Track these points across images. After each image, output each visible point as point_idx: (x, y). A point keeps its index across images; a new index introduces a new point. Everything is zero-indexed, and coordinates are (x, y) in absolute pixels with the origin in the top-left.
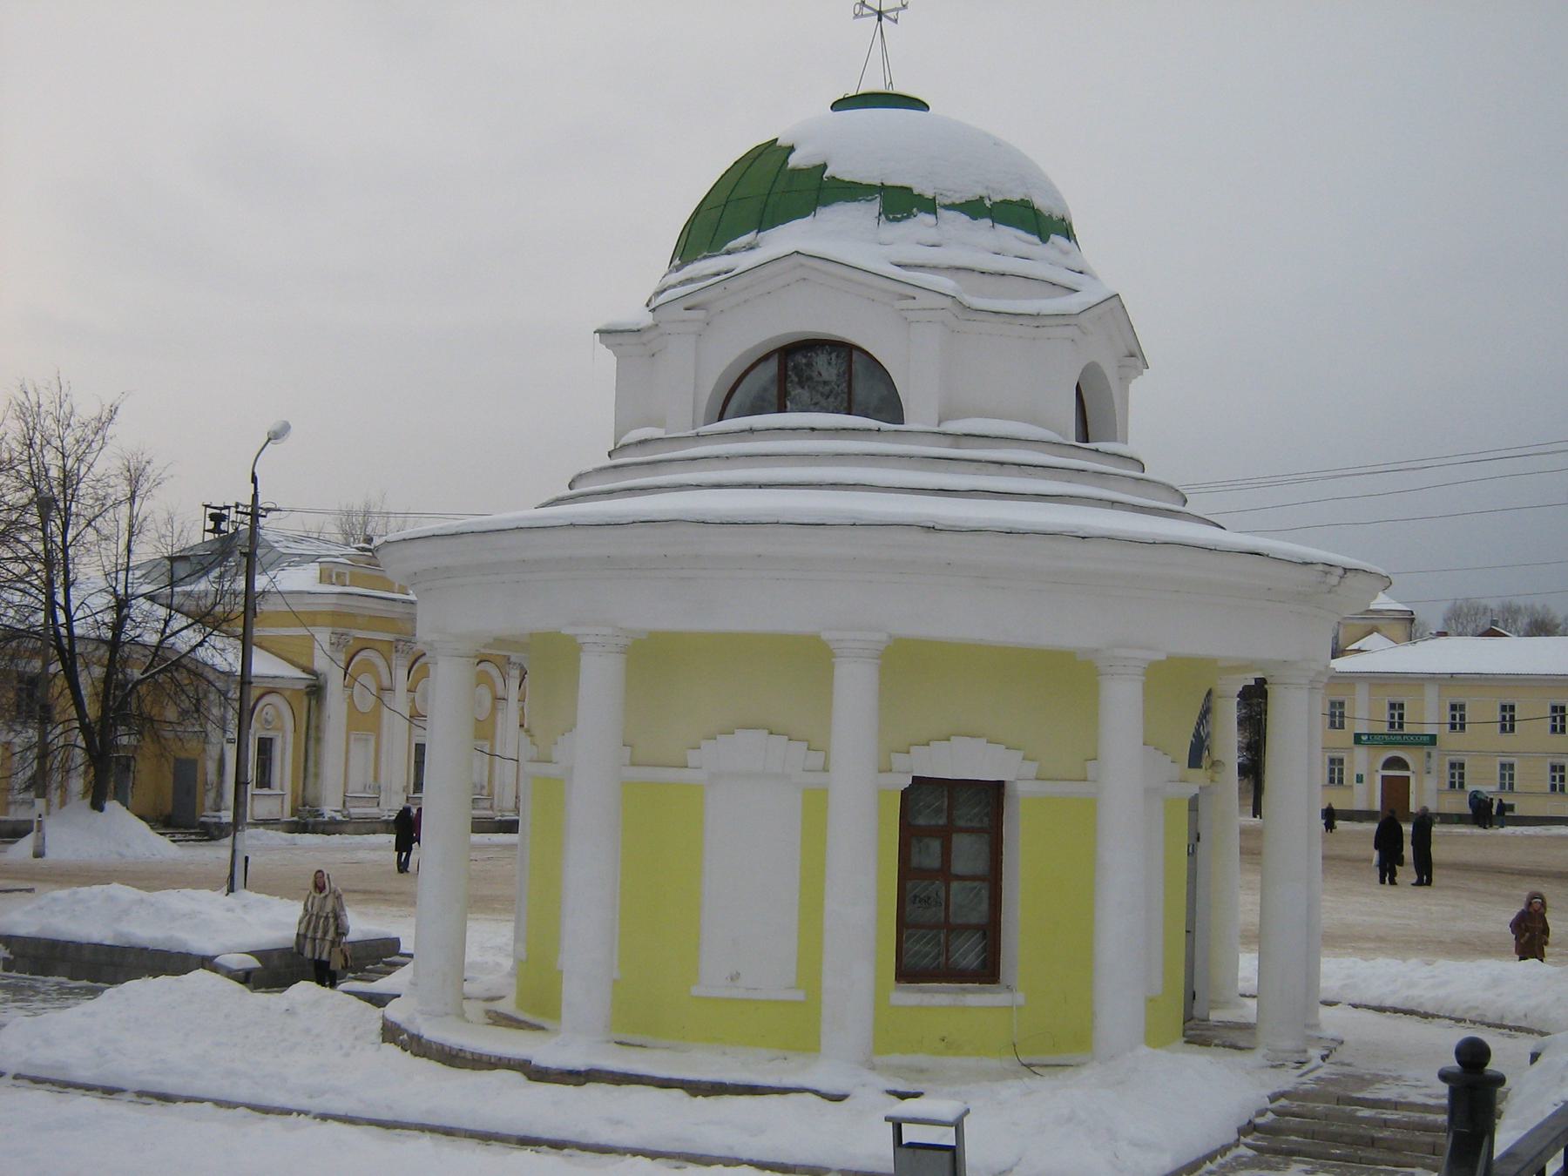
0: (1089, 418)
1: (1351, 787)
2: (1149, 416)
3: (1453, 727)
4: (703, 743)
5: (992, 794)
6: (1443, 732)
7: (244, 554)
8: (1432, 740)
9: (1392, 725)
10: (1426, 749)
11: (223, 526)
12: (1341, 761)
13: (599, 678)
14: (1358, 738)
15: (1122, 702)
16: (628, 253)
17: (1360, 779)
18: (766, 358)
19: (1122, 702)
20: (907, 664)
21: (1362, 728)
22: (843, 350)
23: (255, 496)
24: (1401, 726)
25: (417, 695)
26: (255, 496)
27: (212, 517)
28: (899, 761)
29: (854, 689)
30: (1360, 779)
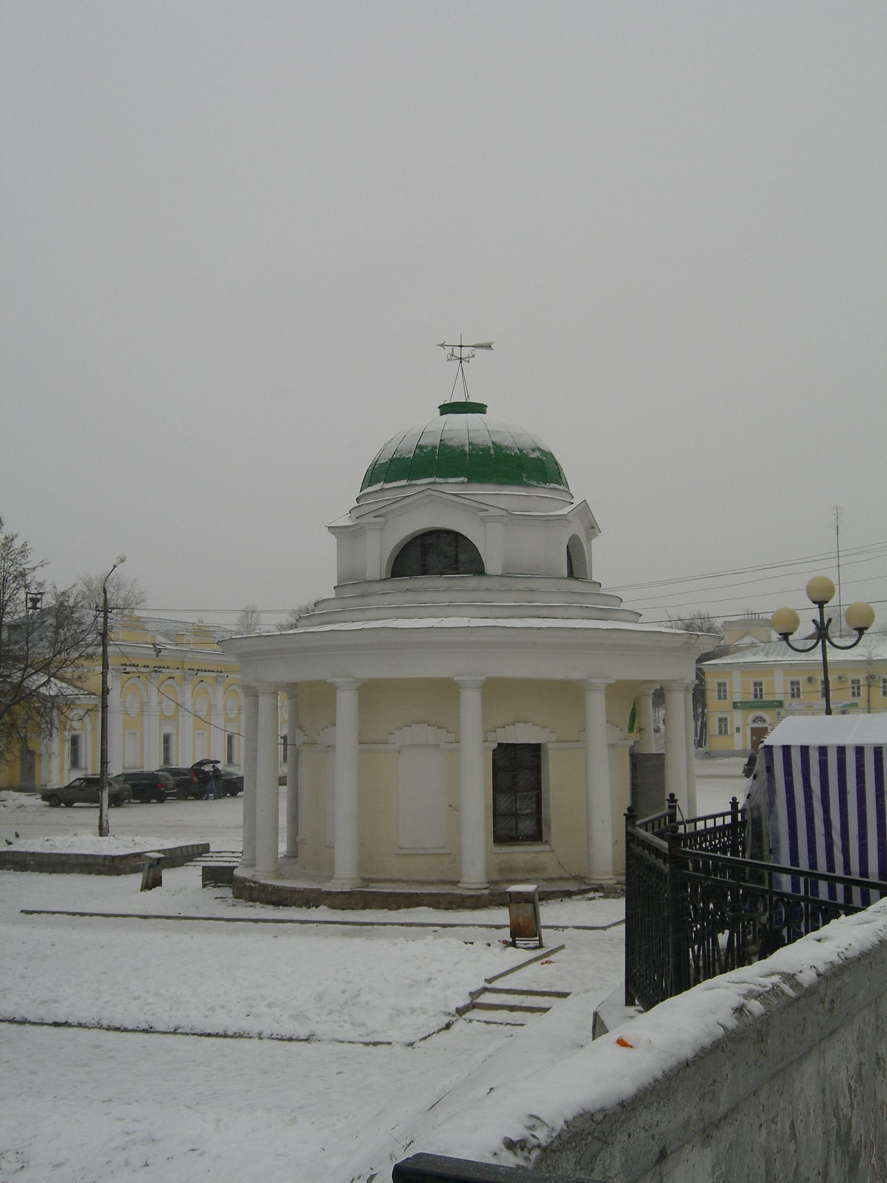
0: (576, 565)
1: (732, 735)
2: (604, 562)
3: (793, 695)
4: (396, 731)
5: (536, 749)
6: (788, 700)
7: (101, 634)
8: (780, 704)
9: (756, 696)
10: (777, 710)
11: (39, 605)
12: (726, 719)
13: (346, 704)
14: (735, 705)
15: (597, 706)
16: (340, 490)
17: (738, 730)
18: (417, 538)
19: (597, 706)
20: (494, 690)
21: (738, 698)
22: (456, 537)
23: (106, 600)
24: (761, 696)
25: (163, 705)
26: (106, 600)
27: (32, 600)
28: (491, 736)
29: (471, 703)
30: (738, 730)
